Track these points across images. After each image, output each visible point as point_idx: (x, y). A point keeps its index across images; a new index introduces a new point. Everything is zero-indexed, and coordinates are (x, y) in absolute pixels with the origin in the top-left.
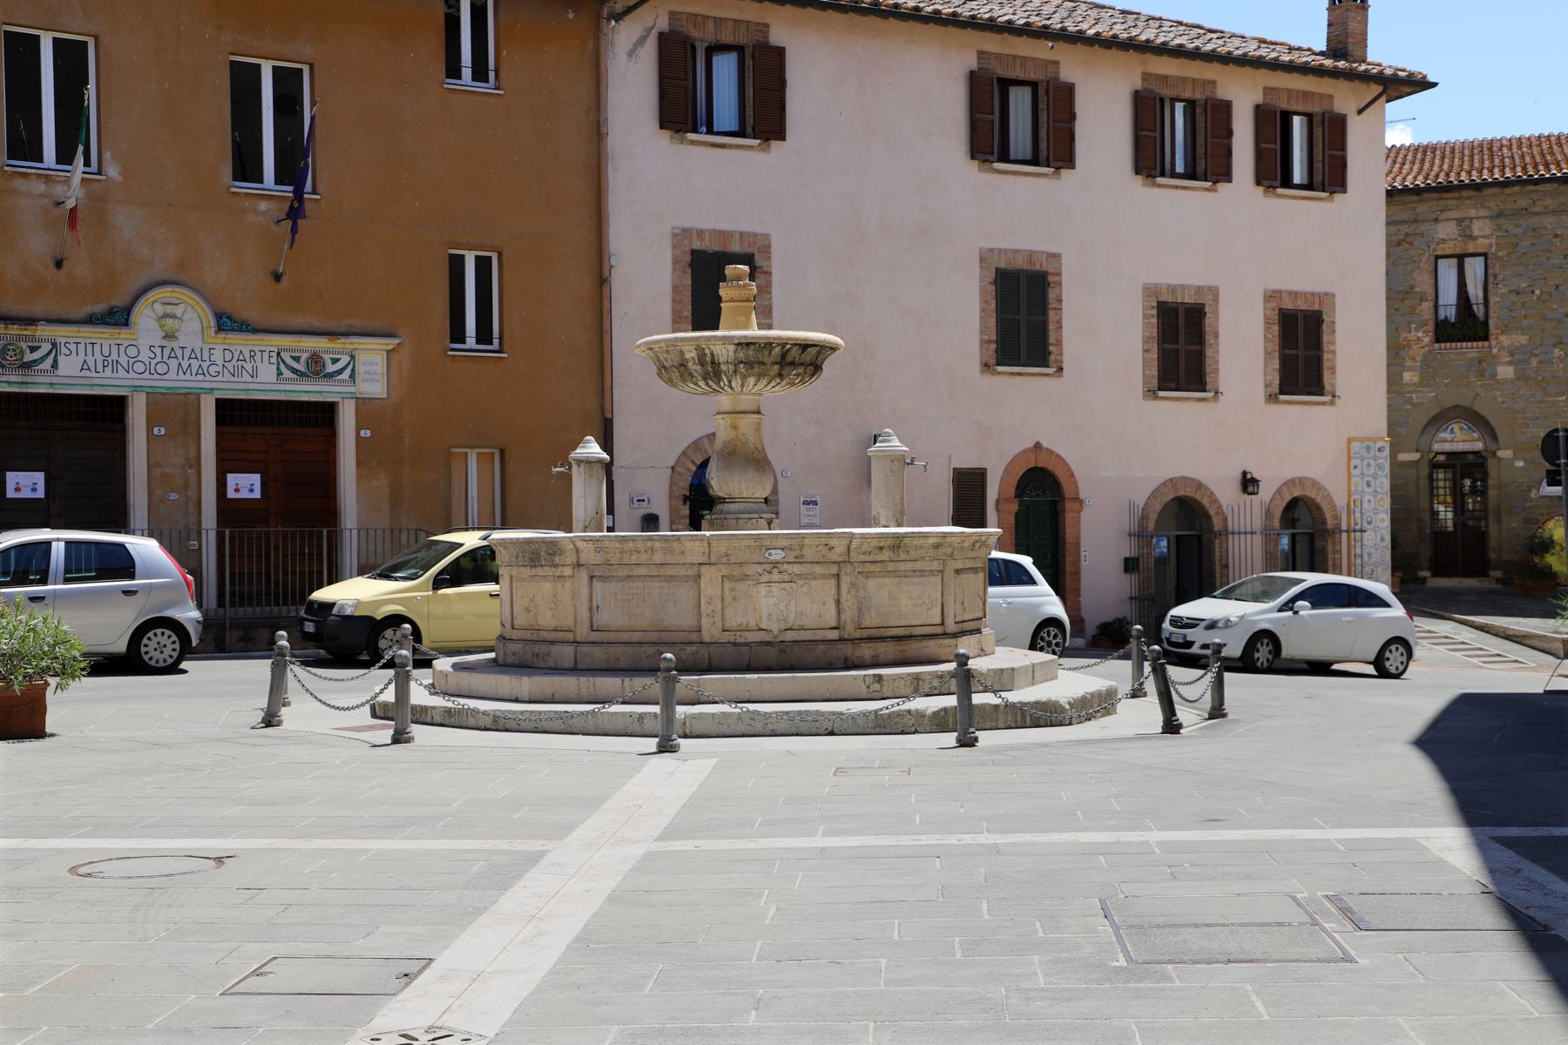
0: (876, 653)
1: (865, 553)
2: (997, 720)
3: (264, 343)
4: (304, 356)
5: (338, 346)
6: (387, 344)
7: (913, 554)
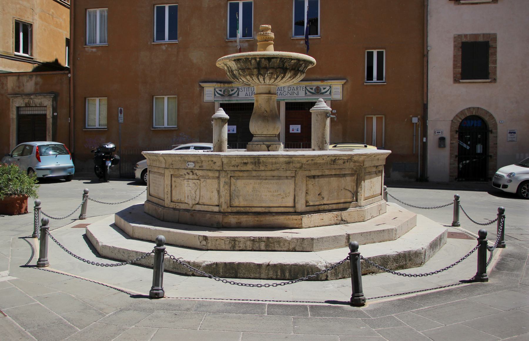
0: (239, 221)
1: (234, 166)
2: (260, 273)
3: (300, 84)
4: (314, 88)
5: (325, 84)
6: (341, 82)
7: (270, 167)
